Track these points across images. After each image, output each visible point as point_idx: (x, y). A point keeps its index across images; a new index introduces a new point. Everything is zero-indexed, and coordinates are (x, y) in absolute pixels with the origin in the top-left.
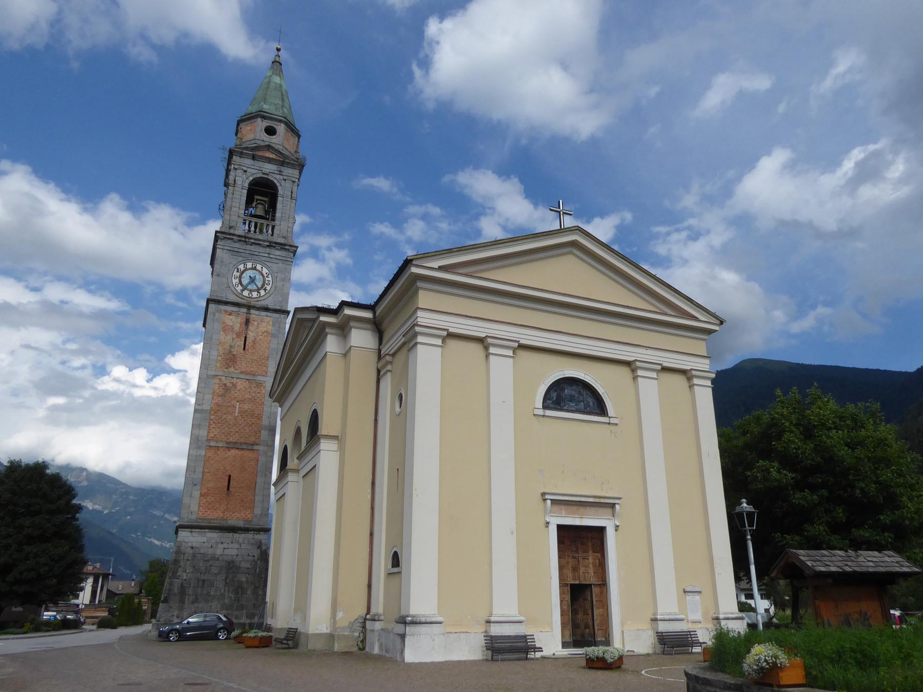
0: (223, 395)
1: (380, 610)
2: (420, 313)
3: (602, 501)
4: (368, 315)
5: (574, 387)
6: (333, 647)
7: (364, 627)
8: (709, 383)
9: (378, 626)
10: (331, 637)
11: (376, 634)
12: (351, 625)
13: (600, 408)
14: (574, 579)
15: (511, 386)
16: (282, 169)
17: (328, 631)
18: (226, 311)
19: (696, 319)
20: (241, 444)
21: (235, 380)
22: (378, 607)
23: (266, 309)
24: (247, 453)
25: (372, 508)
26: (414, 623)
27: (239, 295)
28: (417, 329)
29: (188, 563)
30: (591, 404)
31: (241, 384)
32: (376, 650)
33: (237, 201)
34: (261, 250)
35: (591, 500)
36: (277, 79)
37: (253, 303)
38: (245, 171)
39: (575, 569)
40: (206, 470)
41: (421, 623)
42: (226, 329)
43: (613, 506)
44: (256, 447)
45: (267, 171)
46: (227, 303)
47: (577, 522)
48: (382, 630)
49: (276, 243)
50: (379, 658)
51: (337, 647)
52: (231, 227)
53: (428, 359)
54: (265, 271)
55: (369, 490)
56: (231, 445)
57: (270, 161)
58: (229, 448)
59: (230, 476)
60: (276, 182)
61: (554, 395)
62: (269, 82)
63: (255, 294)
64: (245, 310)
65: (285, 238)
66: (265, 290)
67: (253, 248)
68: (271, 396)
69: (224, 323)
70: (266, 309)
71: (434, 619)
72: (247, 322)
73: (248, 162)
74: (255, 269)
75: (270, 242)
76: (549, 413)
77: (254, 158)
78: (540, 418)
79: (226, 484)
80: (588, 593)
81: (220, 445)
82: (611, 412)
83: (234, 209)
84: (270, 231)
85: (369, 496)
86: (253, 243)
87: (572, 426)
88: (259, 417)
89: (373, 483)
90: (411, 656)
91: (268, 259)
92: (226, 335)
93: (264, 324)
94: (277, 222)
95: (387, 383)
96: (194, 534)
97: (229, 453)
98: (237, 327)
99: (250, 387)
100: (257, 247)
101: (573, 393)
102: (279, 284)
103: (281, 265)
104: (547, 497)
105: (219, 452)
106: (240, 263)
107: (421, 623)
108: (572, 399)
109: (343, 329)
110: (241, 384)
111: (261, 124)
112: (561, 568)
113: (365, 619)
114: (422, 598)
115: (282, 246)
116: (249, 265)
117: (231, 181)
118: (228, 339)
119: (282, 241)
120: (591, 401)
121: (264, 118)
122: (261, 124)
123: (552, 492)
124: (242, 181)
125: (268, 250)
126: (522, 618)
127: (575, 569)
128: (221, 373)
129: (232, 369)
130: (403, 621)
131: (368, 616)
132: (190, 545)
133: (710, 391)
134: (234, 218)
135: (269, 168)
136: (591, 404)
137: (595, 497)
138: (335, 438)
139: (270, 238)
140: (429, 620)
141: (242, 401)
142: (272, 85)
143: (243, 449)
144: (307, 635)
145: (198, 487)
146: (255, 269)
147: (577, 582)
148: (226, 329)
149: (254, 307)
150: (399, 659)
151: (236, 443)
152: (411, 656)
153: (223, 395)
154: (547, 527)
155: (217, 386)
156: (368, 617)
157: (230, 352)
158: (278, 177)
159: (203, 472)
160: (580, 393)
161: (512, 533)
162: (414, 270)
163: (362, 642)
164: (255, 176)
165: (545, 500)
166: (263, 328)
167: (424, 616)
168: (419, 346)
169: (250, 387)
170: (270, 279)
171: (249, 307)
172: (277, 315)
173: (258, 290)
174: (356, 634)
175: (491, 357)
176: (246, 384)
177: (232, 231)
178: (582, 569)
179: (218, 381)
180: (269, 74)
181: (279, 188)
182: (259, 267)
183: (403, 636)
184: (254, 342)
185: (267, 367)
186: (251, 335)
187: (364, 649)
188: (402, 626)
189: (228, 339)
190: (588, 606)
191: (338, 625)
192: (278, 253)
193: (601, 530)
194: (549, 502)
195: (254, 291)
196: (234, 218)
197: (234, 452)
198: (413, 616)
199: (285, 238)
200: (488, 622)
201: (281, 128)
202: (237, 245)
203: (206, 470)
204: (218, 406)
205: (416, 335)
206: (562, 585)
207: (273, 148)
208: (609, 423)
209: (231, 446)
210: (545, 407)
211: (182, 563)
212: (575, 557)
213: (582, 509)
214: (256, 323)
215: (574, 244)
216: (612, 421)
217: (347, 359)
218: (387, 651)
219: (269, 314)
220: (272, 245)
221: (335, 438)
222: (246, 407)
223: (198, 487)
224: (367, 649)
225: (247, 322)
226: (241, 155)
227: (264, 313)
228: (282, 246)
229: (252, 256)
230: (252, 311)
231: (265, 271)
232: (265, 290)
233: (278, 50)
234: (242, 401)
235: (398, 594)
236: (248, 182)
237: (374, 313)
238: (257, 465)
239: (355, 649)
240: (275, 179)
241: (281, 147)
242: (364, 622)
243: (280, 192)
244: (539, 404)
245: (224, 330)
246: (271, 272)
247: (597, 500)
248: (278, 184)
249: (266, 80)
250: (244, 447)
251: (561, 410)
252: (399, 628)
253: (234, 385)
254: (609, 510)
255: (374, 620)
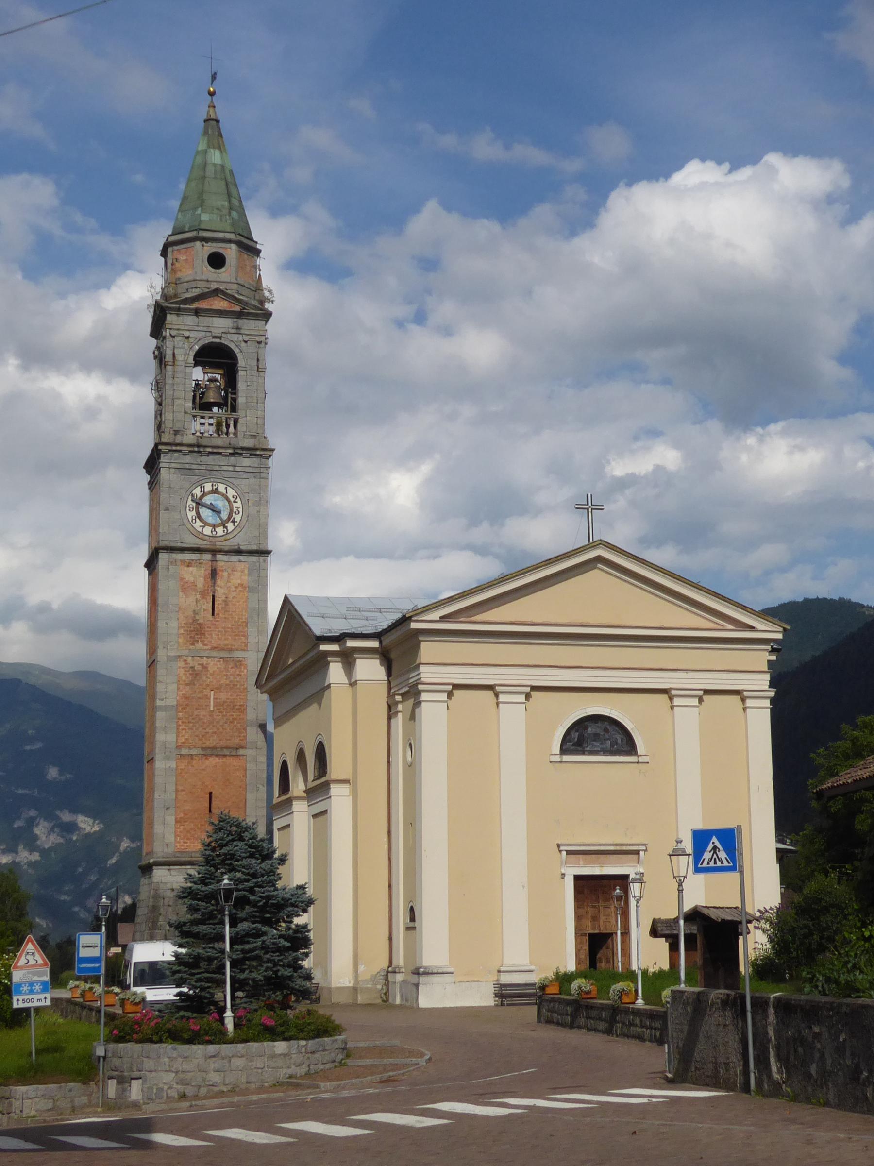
0: (191, 684)
1: (401, 963)
2: (423, 669)
3: (625, 848)
4: (375, 644)
5: (599, 724)
6: (357, 1000)
7: (387, 980)
8: (767, 703)
9: (399, 977)
10: (355, 989)
11: (398, 986)
12: (373, 978)
13: (628, 745)
14: (594, 929)
15: (522, 734)
16: (241, 322)
17: (351, 985)
18: (183, 562)
19: (752, 628)
20: (222, 748)
21: (205, 661)
22: (400, 960)
23: (239, 552)
24: (230, 761)
25: (390, 859)
26: (426, 973)
27: (200, 535)
28: (420, 687)
29: (170, 909)
30: (619, 741)
31: (214, 666)
32: (398, 1001)
33: (181, 388)
34: (222, 461)
35: (612, 848)
36: (215, 157)
37: (219, 545)
38: (187, 338)
39: (595, 919)
40: (180, 788)
41: (433, 973)
42: (186, 587)
43: (637, 852)
44: (241, 752)
45: (217, 332)
46: (182, 550)
47: (597, 871)
48: (403, 981)
49: (243, 449)
50: (401, 1006)
51: (360, 999)
52: (176, 432)
53: (433, 711)
54: (231, 493)
55: (386, 839)
56: (209, 752)
57: (221, 313)
58: (206, 756)
59: (211, 793)
60: (232, 346)
61: (575, 735)
62: (205, 165)
63: (220, 531)
64: (208, 557)
65: (254, 437)
66: (234, 522)
67: (210, 460)
68: (258, 684)
69: (182, 579)
70: (239, 552)
71: (445, 970)
72: (214, 573)
73: (190, 320)
74: (216, 491)
75: (234, 448)
76: (566, 758)
77: (197, 312)
78: (557, 764)
79: (207, 805)
80: (610, 941)
81: (194, 752)
82: (640, 749)
83: (177, 402)
84: (232, 429)
85: (386, 846)
86: (210, 453)
87: (598, 769)
88: (242, 709)
89: (389, 832)
90: (424, 1002)
91: (234, 474)
92: (187, 596)
93: (237, 574)
94: (241, 413)
95: (399, 721)
96: (173, 872)
97: (207, 762)
98: (200, 583)
99: (226, 669)
100: (217, 457)
101: (598, 731)
102: (253, 510)
103: (252, 481)
104: (562, 848)
105: (194, 762)
106: (194, 485)
107: (433, 973)
108: (596, 737)
109: (348, 658)
110: (214, 666)
111: (203, 251)
112: (578, 918)
113: (388, 972)
114: (435, 951)
115: (252, 452)
116: (208, 487)
117: (169, 358)
118: (189, 601)
119: (248, 443)
120: (619, 738)
121: (206, 240)
122: (203, 251)
123: (567, 843)
124: (183, 351)
125: (232, 458)
126: (533, 968)
127: (595, 919)
128: (186, 652)
129: (200, 645)
130: (416, 972)
131: (390, 969)
132: (169, 886)
133: (767, 713)
134: (180, 416)
135: (221, 325)
136: (619, 741)
137: (616, 845)
138: (347, 781)
139: (234, 442)
140: (440, 971)
141: (217, 689)
142: (210, 170)
143: (225, 756)
144: (329, 989)
145: (172, 811)
146: (216, 491)
147: (597, 932)
148: (186, 587)
149: (220, 551)
150: (415, 1005)
151: (215, 748)
152: (424, 1002)
153: (191, 684)
154: (563, 878)
155: (182, 671)
156: (391, 970)
157: (195, 620)
158: (235, 337)
159: (177, 790)
160: (606, 730)
161: (524, 887)
162: (414, 625)
163: (386, 994)
164: (202, 343)
165: (560, 851)
166: (236, 580)
167: (436, 967)
168: (423, 704)
169: (226, 669)
170: (239, 504)
171: (214, 552)
172: (253, 559)
173: (223, 524)
174: (379, 987)
175: (500, 705)
176: (221, 665)
177: (178, 439)
178: (602, 919)
179: (182, 664)
180: (202, 146)
181: (239, 356)
182: (222, 488)
183: (417, 985)
184: (226, 602)
185: (246, 636)
186: (220, 592)
187: (387, 1001)
188: (416, 976)
189: (189, 601)
190: (610, 955)
191: (360, 979)
192: (247, 462)
193: (623, 880)
194: (564, 853)
195: (218, 526)
196: (180, 416)
197: (213, 761)
198: (425, 968)
199: (254, 437)
200: (499, 971)
201: (231, 252)
202: (188, 459)
203: (180, 788)
204: (186, 698)
205: (419, 693)
206: (579, 933)
207: (223, 293)
208: (638, 763)
209: (209, 752)
210: (564, 751)
211: (162, 911)
212: (595, 907)
213: (602, 857)
214: (225, 574)
215: (599, 559)
216: (641, 759)
217: (356, 689)
218: (407, 1001)
219: (241, 558)
220: (237, 451)
221: (347, 781)
222: (223, 696)
223: (172, 811)
224: (390, 1000)
225: (214, 573)
226: (178, 311)
227: (235, 558)
228: (252, 452)
229: (210, 473)
230: (219, 557)
231: (231, 493)
232: (234, 522)
233: (212, 94)
234: (217, 689)
235: (413, 949)
236: (192, 353)
237: (381, 643)
238: (245, 776)
239: (379, 1001)
240: (231, 341)
241: (235, 287)
242: (387, 975)
243: (241, 363)
244: (557, 749)
245: (184, 589)
246: (239, 495)
247: (618, 848)
248: (236, 350)
249: (199, 160)
250: (226, 752)
251: (583, 753)
252: (414, 979)
253: (205, 667)
254: (635, 856)
255: (395, 972)
